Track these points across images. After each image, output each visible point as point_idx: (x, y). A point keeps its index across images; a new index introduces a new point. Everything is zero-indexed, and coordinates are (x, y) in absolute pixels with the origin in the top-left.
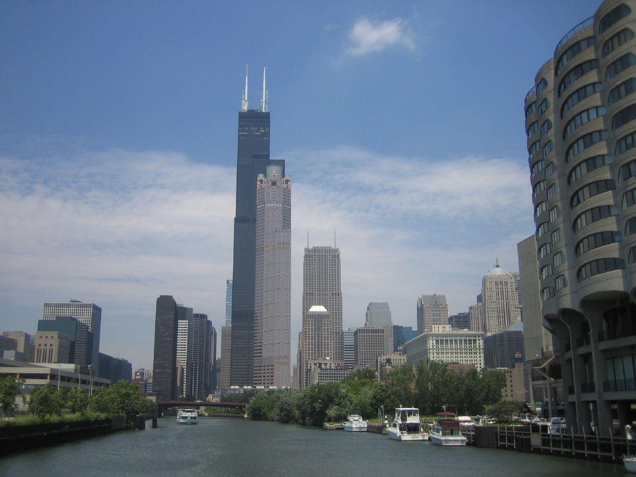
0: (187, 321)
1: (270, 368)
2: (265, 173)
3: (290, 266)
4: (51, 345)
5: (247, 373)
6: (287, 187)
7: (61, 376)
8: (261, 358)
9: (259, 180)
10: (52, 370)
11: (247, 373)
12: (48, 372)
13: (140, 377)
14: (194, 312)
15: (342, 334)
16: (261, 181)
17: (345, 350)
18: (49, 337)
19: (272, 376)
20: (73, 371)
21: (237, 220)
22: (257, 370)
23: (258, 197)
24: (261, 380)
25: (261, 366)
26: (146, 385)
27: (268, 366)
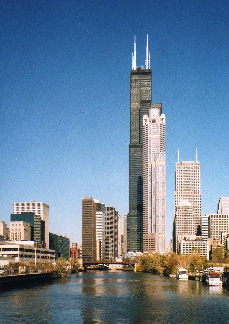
0: (102, 212)
1: (153, 240)
2: (148, 114)
3: (8, 251)
4: (20, 230)
5: (139, 236)
6: (163, 123)
7: (25, 249)
8: (147, 234)
9: (144, 119)
10: (20, 245)
11: (139, 236)
12: (18, 247)
13: (75, 247)
14: (106, 206)
15: (201, 219)
16: (146, 120)
17: (203, 227)
18: (18, 225)
19: (154, 243)
20: (33, 246)
21: (131, 147)
22: (145, 227)
23: (144, 133)
24: (148, 244)
25: (147, 239)
26: (79, 251)
27: (150, 239)
